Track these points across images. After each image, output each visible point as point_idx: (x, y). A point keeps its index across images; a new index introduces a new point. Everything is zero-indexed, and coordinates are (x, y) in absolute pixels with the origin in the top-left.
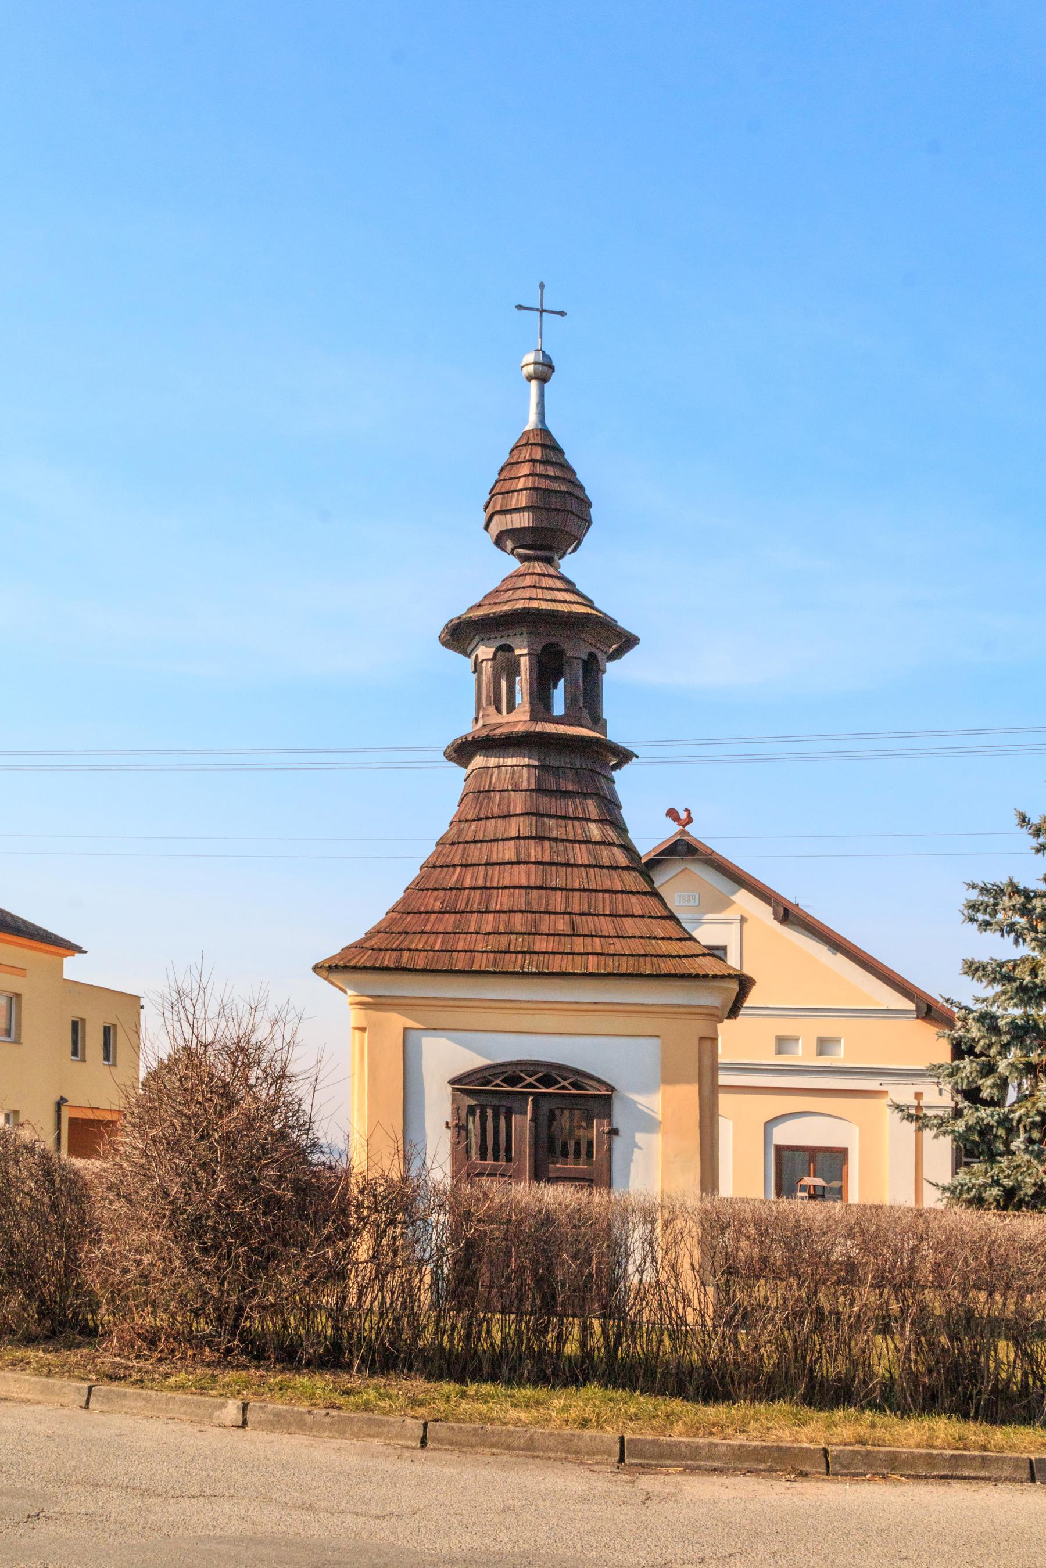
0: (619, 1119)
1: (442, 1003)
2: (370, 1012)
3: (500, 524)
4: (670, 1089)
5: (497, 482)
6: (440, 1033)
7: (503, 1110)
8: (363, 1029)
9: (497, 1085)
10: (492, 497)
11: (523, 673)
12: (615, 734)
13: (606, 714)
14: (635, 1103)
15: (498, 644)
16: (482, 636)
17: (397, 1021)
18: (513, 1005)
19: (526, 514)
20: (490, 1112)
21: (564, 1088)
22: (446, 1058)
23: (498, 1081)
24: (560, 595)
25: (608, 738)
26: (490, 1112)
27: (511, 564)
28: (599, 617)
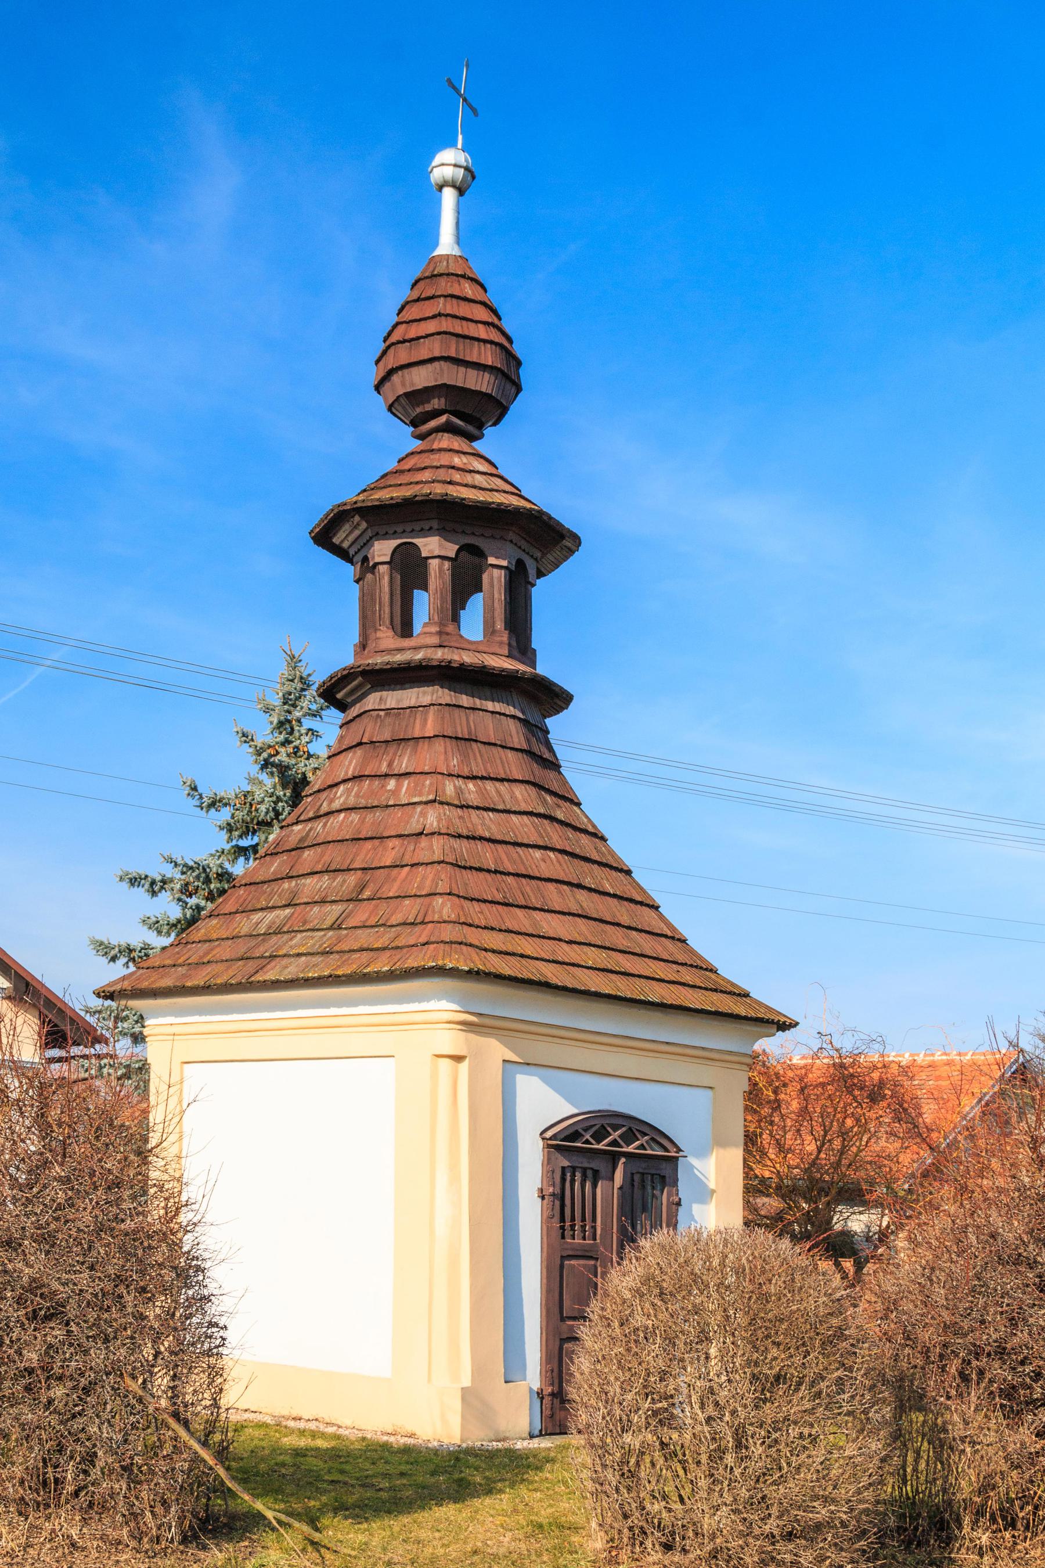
0: (684, 1189)
1: (533, 1028)
2: (472, 1036)
3: (400, 385)
4: (721, 1151)
5: (395, 326)
6: (532, 1069)
7: (589, 1173)
8: (458, 1059)
9: (587, 1142)
10: (389, 347)
11: (433, 582)
12: (548, 666)
13: (537, 641)
14: (693, 1167)
15: (466, 541)
16: (376, 529)
17: (496, 1050)
18: (533, 1028)
19: (487, 375)
20: (578, 1176)
21: (587, 1142)
22: (544, 1104)
23: (588, 1137)
24: (479, 479)
25: (542, 669)
26: (578, 1176)
27: (401, 439)
28: (531, 510)
